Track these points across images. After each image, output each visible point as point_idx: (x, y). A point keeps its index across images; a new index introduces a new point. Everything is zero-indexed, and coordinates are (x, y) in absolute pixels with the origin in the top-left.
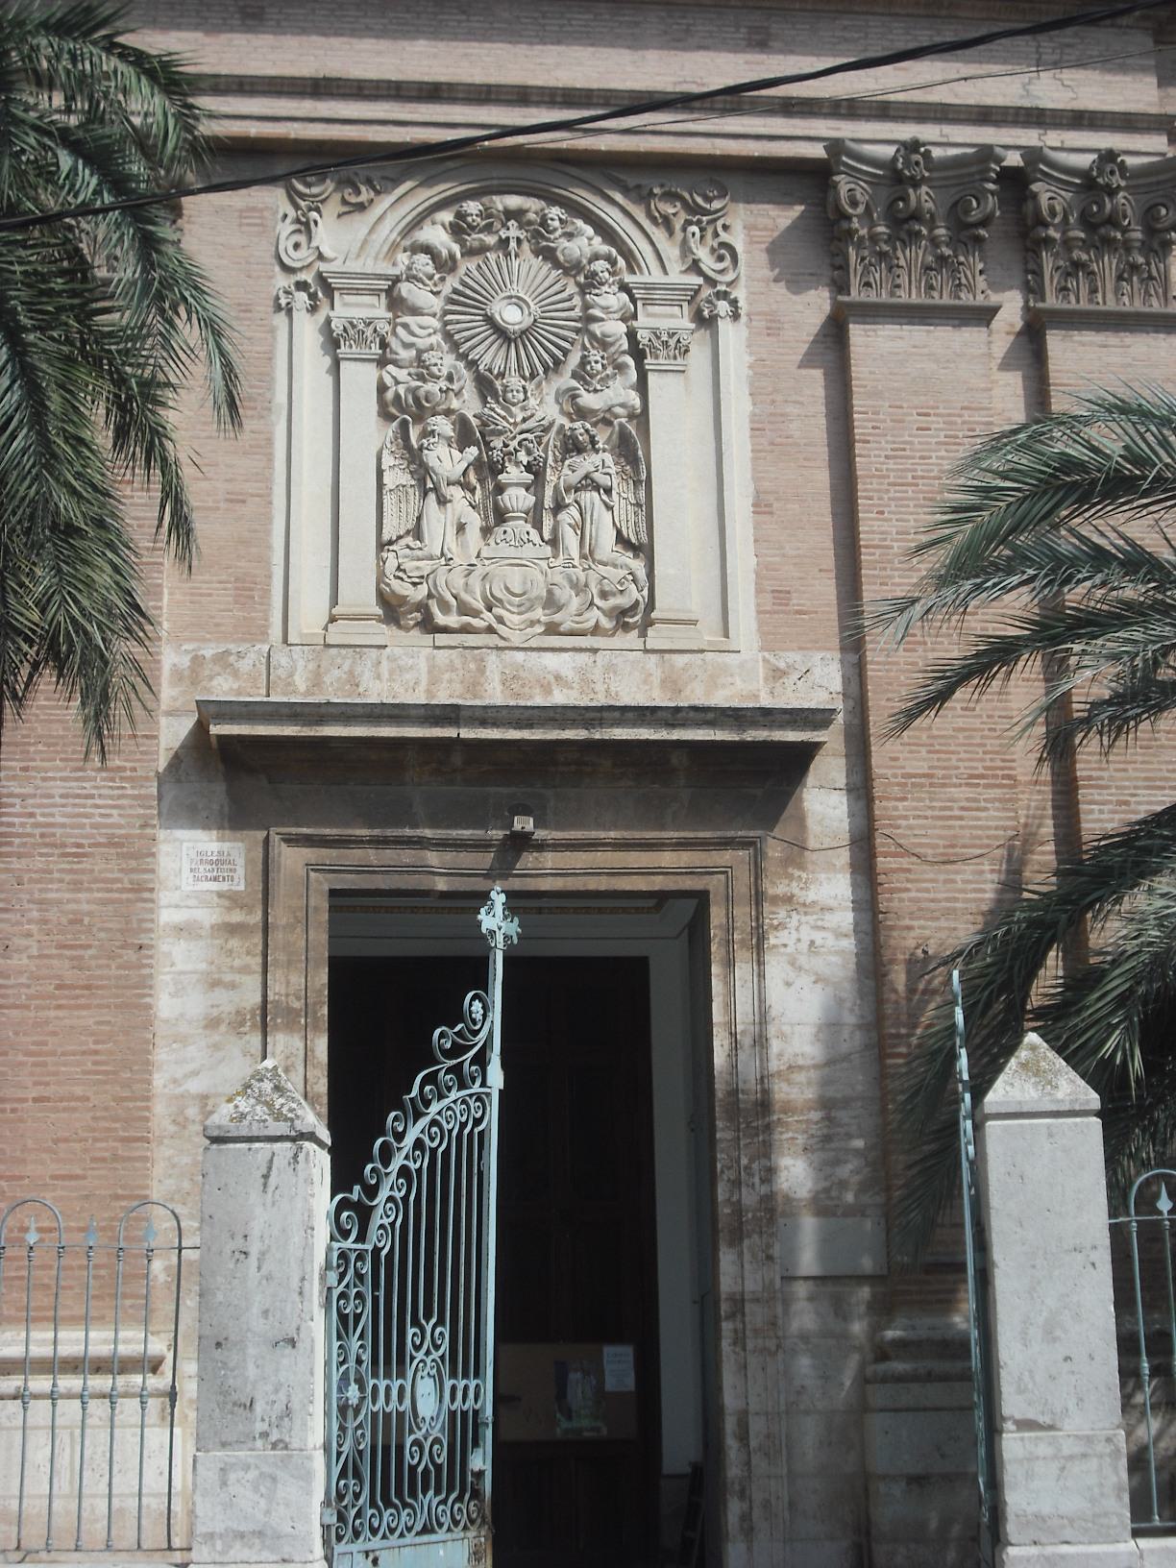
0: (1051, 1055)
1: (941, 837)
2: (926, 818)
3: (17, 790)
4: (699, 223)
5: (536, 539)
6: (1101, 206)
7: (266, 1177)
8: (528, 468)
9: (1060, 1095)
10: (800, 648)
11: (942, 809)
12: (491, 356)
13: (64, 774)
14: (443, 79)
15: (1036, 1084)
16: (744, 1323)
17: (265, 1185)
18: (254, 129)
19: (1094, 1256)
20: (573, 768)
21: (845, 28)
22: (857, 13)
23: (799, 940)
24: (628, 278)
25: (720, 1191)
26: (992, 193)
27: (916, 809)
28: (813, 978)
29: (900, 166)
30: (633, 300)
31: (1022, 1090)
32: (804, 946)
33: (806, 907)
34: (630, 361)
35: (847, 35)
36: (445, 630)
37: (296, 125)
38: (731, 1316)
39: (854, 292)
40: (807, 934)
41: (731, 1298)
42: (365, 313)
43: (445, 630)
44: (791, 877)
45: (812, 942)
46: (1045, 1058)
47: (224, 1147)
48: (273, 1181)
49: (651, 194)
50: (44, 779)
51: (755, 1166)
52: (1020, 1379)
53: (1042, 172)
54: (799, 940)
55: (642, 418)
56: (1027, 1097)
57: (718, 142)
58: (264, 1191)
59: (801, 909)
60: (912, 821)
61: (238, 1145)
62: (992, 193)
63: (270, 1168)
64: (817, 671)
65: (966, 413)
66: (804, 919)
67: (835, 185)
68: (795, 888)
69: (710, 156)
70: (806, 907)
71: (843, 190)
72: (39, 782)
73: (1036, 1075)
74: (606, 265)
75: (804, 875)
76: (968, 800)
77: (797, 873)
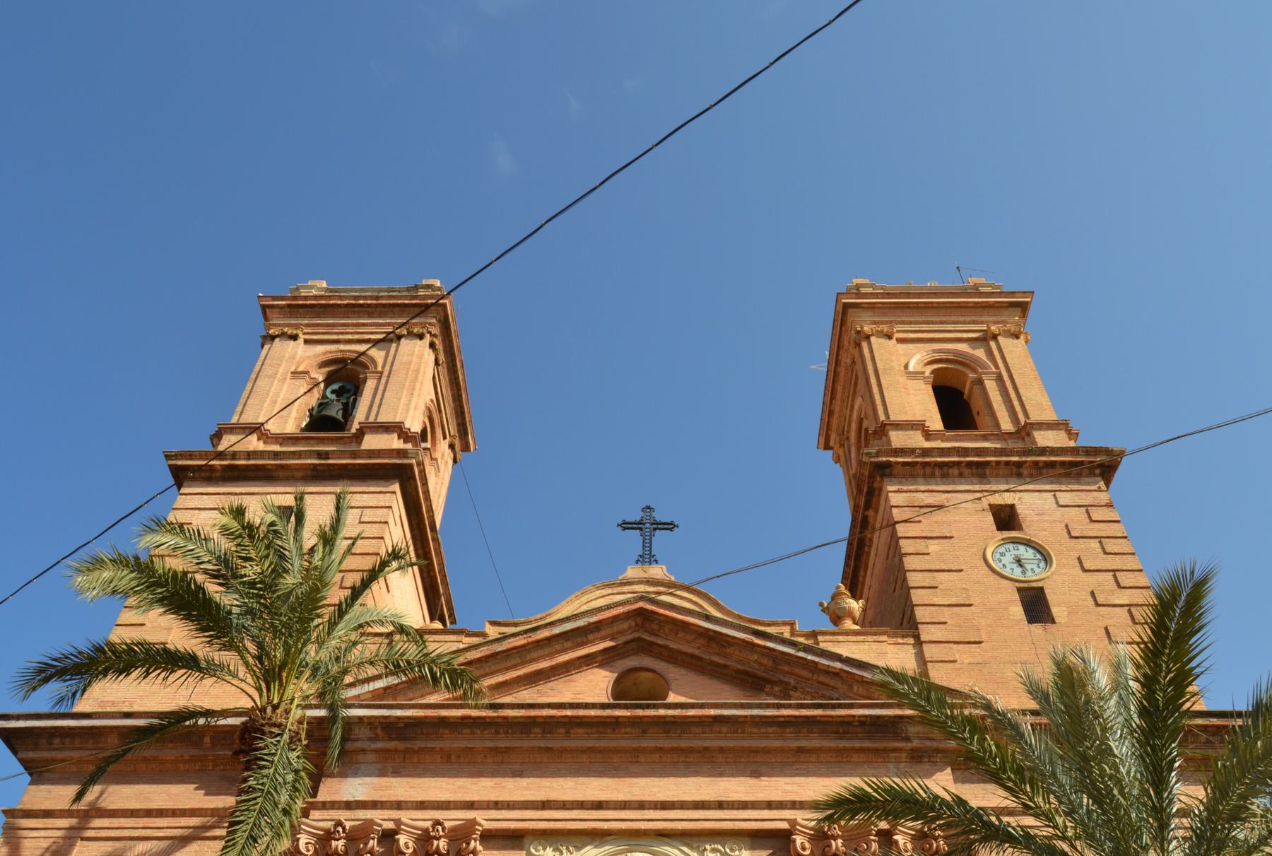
6: (931, 845)
14: (603, 799)
18: (513, 825)
21: (797, 769)
22: (803, 762)
26: (874, 841)
29: (826, 830)
35: (797, 772)
37: (533, 823)
49: (705, 849)
53: (900, 831)
57: (737, 823)
62: (874, 841)
67: (794, 841)
69: (733, 830)
71: (402, 843)
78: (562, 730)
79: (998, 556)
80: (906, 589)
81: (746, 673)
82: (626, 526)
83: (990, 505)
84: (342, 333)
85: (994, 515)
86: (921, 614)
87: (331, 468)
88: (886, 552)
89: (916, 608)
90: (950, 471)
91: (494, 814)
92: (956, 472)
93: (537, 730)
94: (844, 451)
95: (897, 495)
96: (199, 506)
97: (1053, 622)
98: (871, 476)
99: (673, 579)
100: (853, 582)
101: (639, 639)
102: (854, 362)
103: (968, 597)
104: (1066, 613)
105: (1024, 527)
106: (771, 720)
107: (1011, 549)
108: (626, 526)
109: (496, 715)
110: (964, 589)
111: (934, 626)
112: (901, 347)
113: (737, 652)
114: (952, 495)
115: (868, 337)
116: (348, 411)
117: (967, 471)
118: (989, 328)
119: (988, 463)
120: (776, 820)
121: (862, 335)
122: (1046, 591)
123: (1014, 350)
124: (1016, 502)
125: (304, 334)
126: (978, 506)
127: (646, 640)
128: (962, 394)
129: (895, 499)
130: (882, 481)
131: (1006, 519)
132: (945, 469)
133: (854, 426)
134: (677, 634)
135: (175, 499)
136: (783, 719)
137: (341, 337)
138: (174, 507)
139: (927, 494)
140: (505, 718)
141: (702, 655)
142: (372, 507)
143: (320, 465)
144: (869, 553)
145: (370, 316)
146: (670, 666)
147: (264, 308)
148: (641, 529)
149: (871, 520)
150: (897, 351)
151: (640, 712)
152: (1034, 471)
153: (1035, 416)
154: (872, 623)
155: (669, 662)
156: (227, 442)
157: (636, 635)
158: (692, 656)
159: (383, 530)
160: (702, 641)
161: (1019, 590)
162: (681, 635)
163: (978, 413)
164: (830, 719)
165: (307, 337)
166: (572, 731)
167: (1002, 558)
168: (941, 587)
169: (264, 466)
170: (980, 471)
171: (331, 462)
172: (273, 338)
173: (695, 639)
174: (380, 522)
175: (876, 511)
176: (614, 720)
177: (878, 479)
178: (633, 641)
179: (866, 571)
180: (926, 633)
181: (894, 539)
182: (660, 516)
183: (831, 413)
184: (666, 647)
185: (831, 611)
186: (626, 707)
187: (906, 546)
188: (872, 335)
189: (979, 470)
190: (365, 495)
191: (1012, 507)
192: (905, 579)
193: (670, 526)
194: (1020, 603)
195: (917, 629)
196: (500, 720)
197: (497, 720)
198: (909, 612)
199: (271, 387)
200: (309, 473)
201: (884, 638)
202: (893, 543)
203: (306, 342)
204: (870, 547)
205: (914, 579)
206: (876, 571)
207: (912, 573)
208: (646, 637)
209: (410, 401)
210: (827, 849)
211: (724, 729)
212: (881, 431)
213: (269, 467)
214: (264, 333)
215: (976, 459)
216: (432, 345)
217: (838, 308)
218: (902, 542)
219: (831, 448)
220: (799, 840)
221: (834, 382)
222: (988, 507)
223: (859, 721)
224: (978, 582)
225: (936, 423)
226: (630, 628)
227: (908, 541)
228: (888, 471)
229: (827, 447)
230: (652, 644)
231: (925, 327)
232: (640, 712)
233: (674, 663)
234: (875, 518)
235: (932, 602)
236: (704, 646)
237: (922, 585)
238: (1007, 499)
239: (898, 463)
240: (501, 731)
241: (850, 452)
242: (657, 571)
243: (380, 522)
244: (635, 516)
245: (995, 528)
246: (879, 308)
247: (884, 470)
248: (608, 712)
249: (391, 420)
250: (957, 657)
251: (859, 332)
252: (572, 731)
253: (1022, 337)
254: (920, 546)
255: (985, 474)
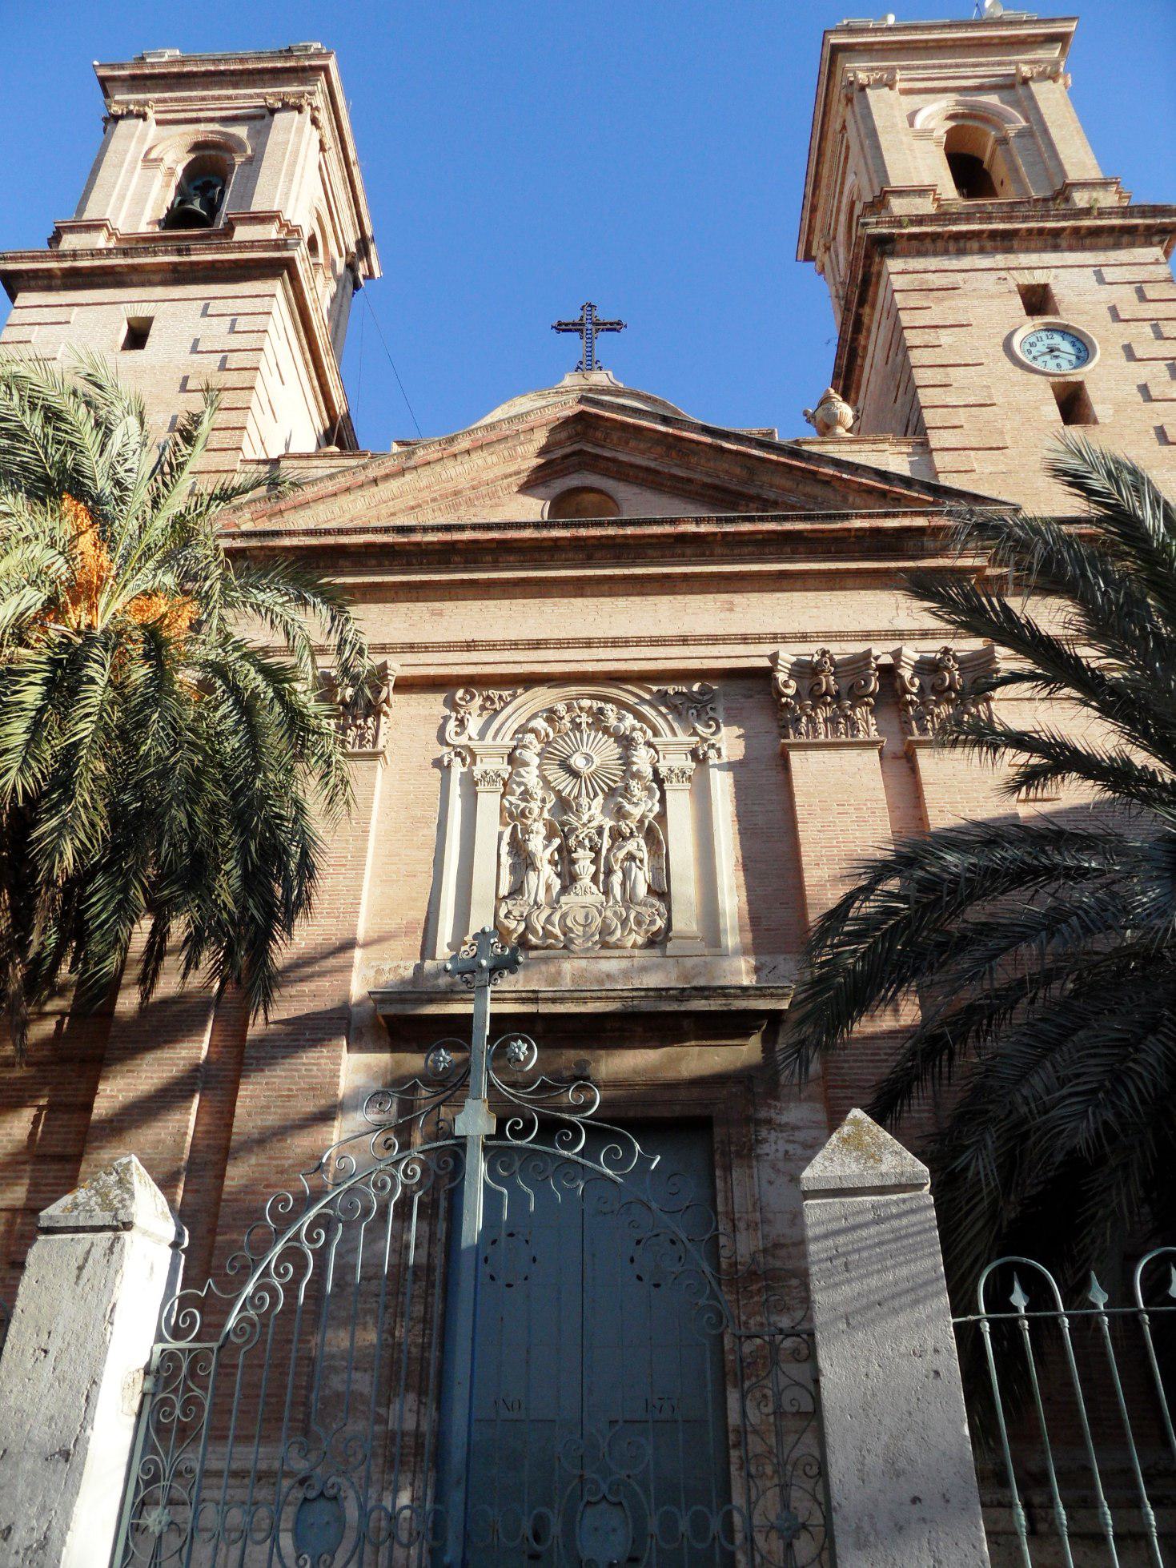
0: (877, 1128)
1: (873, 1074)
2: (862, 1061)
3: (255, 1055)
4: (695, 708)
5: (596, 892)
7: (80, 1268)
8: (591, 849)
9: (884, 1168)
10: (769, 953)
11: (872, 1054)
12: (566, 784)
13: (285, 1043)
15: (857, 1160)
16: (746, 1451)
17: (78, 1277)
19: (939, 1363)
20: (617, 1034)
23: (777, 1150)
24: (653, 740)
25: (726, 1342)
27: (853, 1055)
28: (788, 1178)
30: (657, 752)
31: (842, 1164)
32: (780, 1155)
33: (782, 1127)
34: (655, 785)
36: (536, 948)
37: (457, 667)
38: (737, 1445)
39: (792, 736)
40: (782, 1146)
41: (737, 1431)
42: (495, 767)
43: (536, 948)
44: (769, 1106)
45: (787, 1152)
46: (869, 1132)
47: (52, 1237)
48: (85, 1273)
50: (272, 1047)
51: (752, 1322)
52: (859, 1528)
54: (777, 1150)
55: (662, 817)
56: (848, 1172)
58: (76, 1283)
59: (778, 1129)
60: (852, 1064)
61: (64, 1236)
63: (86, 1260)
64: (781, 967)
65: (868, 803)
66: (780, 1135)
68: (772, 1114)
70: (782, 1127)
72: (270, 1049)
73: (857, 1149)
74: (640, 733)
75: (778, 1104)
76: (890, 1048)
77: (774, 1103)
78: (489, 558)
79: (1027, 347)
80: (912, 390)
81: (715, 487)
82: (562, 327)
83: (1018, 285)
84: (201, 110)
85: (1023, 297)
86: (929, 417)
87: (195, 267)
88: (885, 355)
89: (924, 410)
90: (968, 245)
91: (409, 658)
92: (975, 245)
93: (457, 559)
94: (830, 257)
95: (900, 276)
96: (39, 321)
97: (1096, 422)
98: (868, 257)
99: (621, 385)
100: (847, 380)
101: (580, 452)
102: (844, 127)
103: (990, 397)
104: (1111, 412)
105: (1060, 309)
106: (746, 537)
107: (1044, 338)
108: (562, 327)
109: (406, 540)
110: (985, 386)
111: (947, 431)
112: (904, 98)
113: (703, 461)
114: (971, 274)
115: (863, 88)
116: (213, 207)
117: (989, 244)
118: (1018, 69)
119: (1016, 232)
120: (754, 657)
121: (856, 86)
122: (1087, 386)
123: (1051, 98)
124: (1050, 281)
125: (156, 112)
126: (1003, 288)
127: (589, 453)
128: (982, 162)
129: (897, 282)
130: (882, 263)
131: (1037, 300)
132: (961, 244)
133: (843, 218)
134: (627, 443)
135: (9, 314)
136: (760, 536)
137: (201, 114)
138: (9, 322)
139: (937, 274)
140: (418, 544)
141: (658, 468)
142: (248, 314)
143: (181, 263)
144: (862, 367)
145: (236, 86)
146: (621, 484)
147: (103, 81)
148: (581, 331)
149: (866, 320)
150: (900, 105)
151: (583, 532)
152: (1074, 242)
153: (1073, 176)
154: (865, 430)
155: (620, 480)
156: (69, 242)
157: (576, 447)
158: (648, 469)
159: (262, 340)
160: (659, 450)
161: (1054, 387)
162: (632, 443)
163: (1002, 183)
164: (821, 535)
165: (161, 116)
166: (500, 559)
167: (1032, 349)
168: (955, 385)
169: (113, 267)
170: (1006, 243)
171: (194, 258)
172: (116, 118)
173: (650, 448)
174: (258, 331)
175: (873, 307)
176: (551, 543)
177: (877, 259)
178: (574, 454)
179: (857, 393)
180: (936, 439)
181: (898, 330)
182: (602, 315)
183: (814, 209)
184: (614, 460)
185: (818, 419)
186: (565, 526)
187: (912, 338)
188: (868, 85)
189: (1005, 241)
190: (238, 300)
191: (1046, 287)
192: (910, 378)
193: (615, 327)
194: (1055, 401)
195: (926, 434)
196: (411, 548)
197: (408, 547)
198: (915, 419)
199: (117, 177)
200: (169, 276)
201: (885, 446)
202: (896, 335)
203: (159, 123)
204: (864, 358)
205: (921, 376)
206: (872, 387)
207: (919, 370)
208: (589, 448)
209: (289, 189)
210: (816, 688)
211: (688, 551)
212: (880, 202)
213: (119, 269)
214: (104, 114)
215: (1001, 226)
216: (314, 121)
217: (824, 56)
218: (906, 333)
219: (813, 259)
220: (782, 677)
221: (818, 164)
222: (1016, 289)
223: (856, 537)
224: (1002, 378)
225: (948, 189)
226: (569, 438)
227: (914, 331)
228: (889, 247)
229: (808, 257)
230: (597, 457)
231: (935, 73)
232: (583, 532)
233: (623, 480)
234: (872, 315)
235: (944, 403)
236: (662, 457)
237: (932, 383)
238: (1039, 278)
239: (902, 235)
240: (414, 561)
241: (837, 256)
242: (599, 378)
243: (258, 331)
244: (575, 317)
245: (1024, 312)
246: (877, 50)
247: (884, 246)
248: (545, 533)
249: (268, 209)
250: (976, 466)
251: (851, 83)
252: (500, 559)
253: (1061, 81)
254: (929, 337)
255: (1012, 248)
